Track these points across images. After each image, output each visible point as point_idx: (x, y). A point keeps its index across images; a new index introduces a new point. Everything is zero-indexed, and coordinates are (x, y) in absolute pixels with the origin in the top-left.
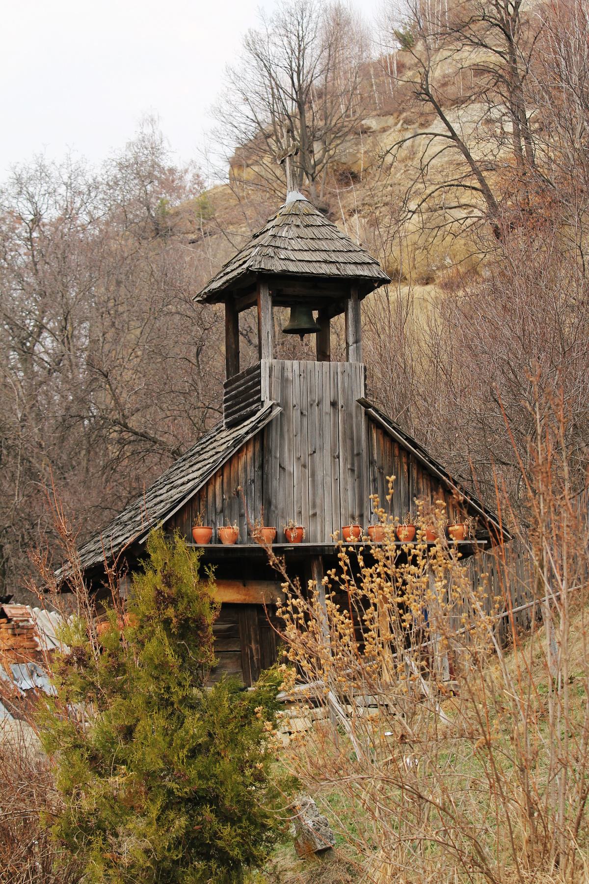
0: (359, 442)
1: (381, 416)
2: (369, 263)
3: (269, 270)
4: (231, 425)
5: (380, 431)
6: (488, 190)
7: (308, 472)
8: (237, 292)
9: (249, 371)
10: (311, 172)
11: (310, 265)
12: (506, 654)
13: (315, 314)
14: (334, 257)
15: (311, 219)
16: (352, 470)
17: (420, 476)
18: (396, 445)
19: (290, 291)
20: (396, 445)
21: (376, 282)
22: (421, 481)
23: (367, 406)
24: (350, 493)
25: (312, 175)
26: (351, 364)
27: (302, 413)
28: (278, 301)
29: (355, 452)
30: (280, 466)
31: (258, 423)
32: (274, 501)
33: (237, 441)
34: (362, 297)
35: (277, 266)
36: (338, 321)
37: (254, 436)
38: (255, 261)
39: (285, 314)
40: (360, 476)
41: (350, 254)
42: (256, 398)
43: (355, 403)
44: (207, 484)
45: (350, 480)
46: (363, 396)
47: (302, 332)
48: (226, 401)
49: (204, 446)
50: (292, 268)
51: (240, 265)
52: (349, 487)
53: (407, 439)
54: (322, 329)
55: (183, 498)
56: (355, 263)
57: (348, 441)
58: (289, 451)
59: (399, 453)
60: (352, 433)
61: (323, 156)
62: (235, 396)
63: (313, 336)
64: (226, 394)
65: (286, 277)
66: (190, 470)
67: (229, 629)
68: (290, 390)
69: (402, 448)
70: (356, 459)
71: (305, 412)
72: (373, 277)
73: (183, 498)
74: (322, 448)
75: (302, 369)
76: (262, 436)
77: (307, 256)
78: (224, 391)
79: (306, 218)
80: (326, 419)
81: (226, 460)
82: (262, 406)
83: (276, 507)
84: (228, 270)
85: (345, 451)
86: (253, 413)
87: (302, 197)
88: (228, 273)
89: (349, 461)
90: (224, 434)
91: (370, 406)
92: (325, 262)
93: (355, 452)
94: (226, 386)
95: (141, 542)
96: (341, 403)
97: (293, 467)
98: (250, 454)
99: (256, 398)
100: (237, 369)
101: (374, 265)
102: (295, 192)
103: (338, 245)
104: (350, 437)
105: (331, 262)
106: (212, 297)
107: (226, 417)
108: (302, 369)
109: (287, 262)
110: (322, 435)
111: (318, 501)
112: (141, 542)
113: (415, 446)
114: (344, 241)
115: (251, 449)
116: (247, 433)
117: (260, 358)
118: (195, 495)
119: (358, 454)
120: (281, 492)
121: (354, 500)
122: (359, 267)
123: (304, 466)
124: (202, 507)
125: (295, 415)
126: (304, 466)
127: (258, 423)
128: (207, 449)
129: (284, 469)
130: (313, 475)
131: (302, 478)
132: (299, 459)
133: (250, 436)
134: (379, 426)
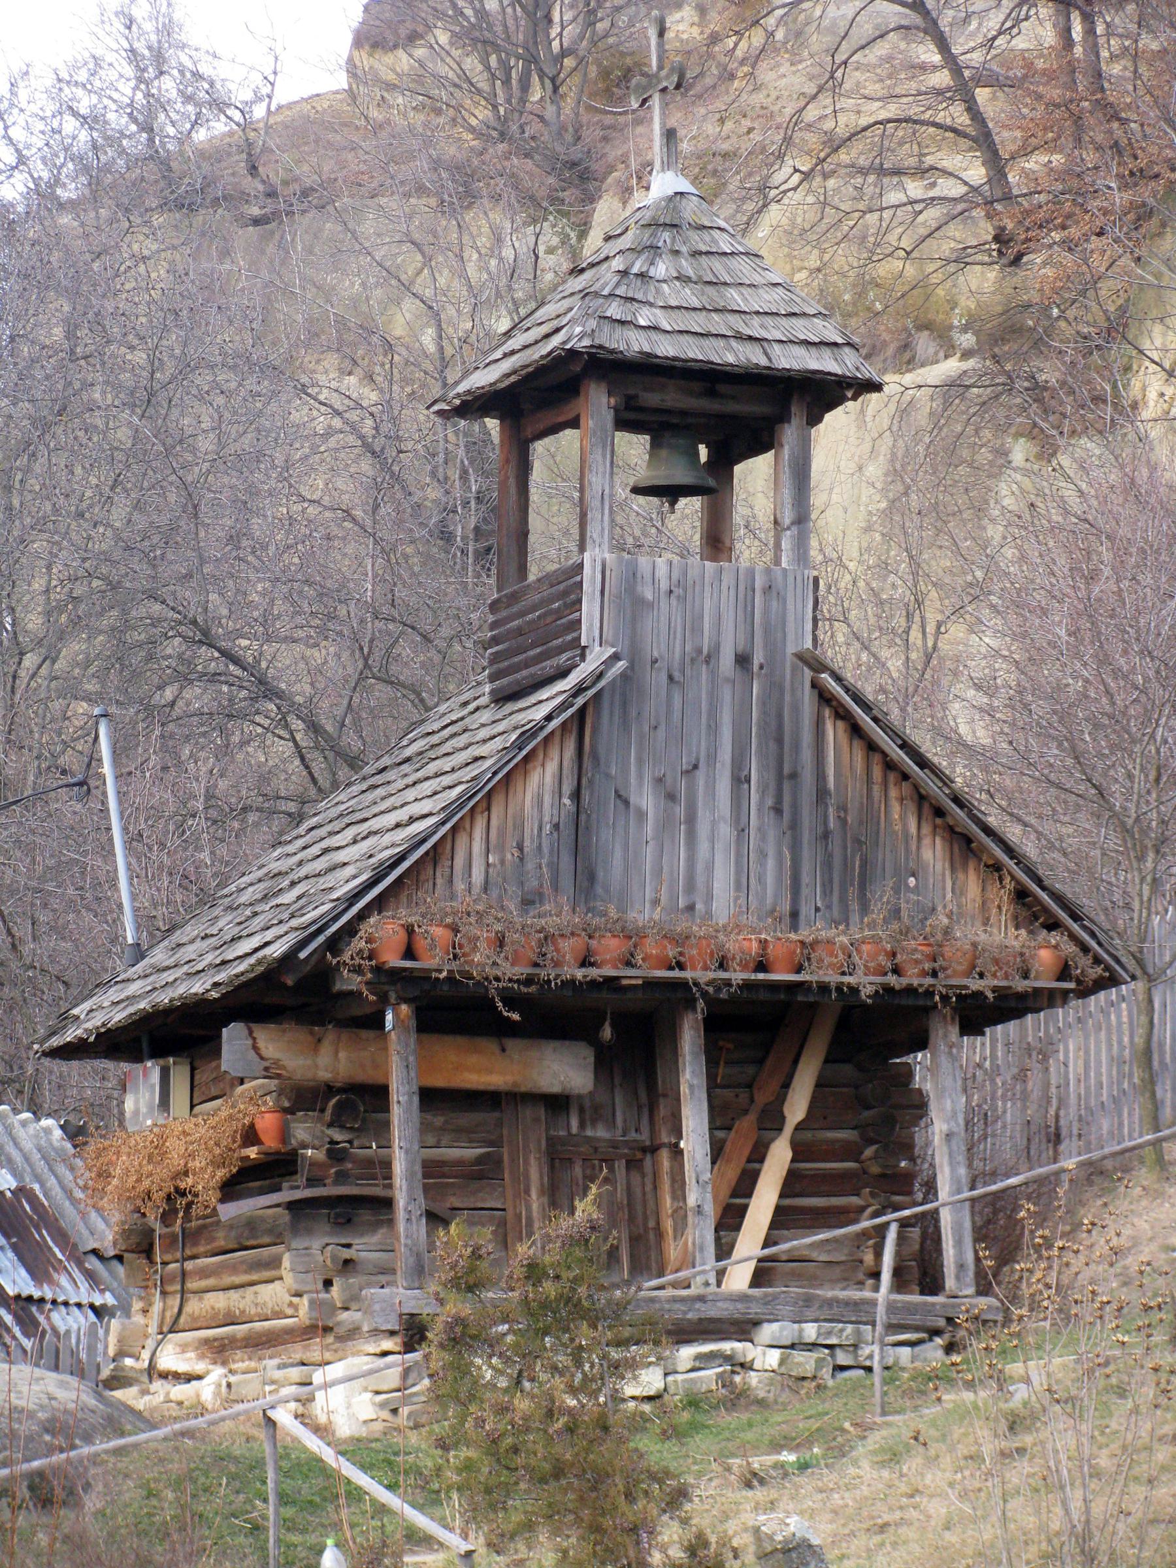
0: (796, 747)
1: (847, 690)
2: (835, 344)
3: (612, 351)
4: (503, 698)
5: (841, 724)
6: (988, 134)
7: (680, 811)
8: (536, 399)
9: (550, 579)
10: (550, 71)
11: (707, 343)
12: (374, 1404)
13: (703, 452)
14: (755, 328)
15: (707, 238)
16: (778, 810)
17: (926, 829)
18: (877, 758)
19: (652, 399)
20: (877, 758)
21: (850, 386)
22: (927, 841)
23: (818, 666)
24: (771, 863)
25: (553, 80)
26: (785, 570)
27: (671, 678)
28: (629, 419)
29: (787, 770)
30: (618, 796)
31: (575, 695)
32: (600, 874)
33: (528, 735)
34: (814, 419)
35: (634, 343)
36: (755, 477)
37: (564, 724)
38: (576, 335)
39: (634, 449)
40: (794, 826)
41: (794, 320)
42: (569, 637)
43: (789, 659)
44: (454, 829)
45: (772, 835)
46: (809, 644)
47: (671, 493)
48: (495, 641)
49: (435, 739)
50: (666, 348)
51: (547, 336)
52: (771, 851)
53: (905, 746)
54: (714, 486)
55: (401, 858)
56: (807, 343)
57: (772, 745)
58: (640, 761)
59: (885, 777)
60: (780, 727)
61: (582, 37)
62: (519, 632)
63: (691, 506)
64: (494, 626)
65: (649, 368)
66: (410, 794)
67: (480, 1160)
68: (648, 623)
69: (890, 765)
70: (787, 786)
71: (677, 675)
72: (844, 376)
73: (401, 858)
74: (712, 758)
75: (675, 576)
76: (579, 721)
77: (697, 323)
78: (491, 618)
79: (694, 236)
80: (726, 694)
81: (500, 776)
82: (583, 657)
83: (607, 891)
84: (513, 344)
85: (762, 768)
86: (563, 674)
87: (685, 186)
88: (513, 353)
89: (772, 790)
90: (485, 716)
91: (824, 668)
92: (739, 337)
93: (787, 770)
94: (494, 607)
95: (302, 955)
96: (758, 658)
97: (646, 799)
98: (552, 767)
99: (569, 637)
100: (523, 570)
101: (847, 350)
102: (670, 174)
103: (769, 300)
104: (777, 736)
105: (750, 338)
106: (474, 406)
107: (492, 678)
108: (675, 576)
109: (654, 335)
110: (713, 729)
111: (700, 880)
112: (302, 955)
113: (923, 763)
114: (780, 290)
115: (554, 753)
116: (549, 718)
117: (582, 548)
118: (427, 853)
119: (794, 776)
120: (618, 854)
121: (779, 879)
122: (813, 350)
123: (671, 797)
124: (439, 881)
125: (656, 681)
126: (671, 797)
127: (575, 695)
128: (447, 747)
129: (626, 803)
130: (691, 820)
131: (666, 824)
132: (660, 781)
133: (555, 723)
134: (842, 714)
